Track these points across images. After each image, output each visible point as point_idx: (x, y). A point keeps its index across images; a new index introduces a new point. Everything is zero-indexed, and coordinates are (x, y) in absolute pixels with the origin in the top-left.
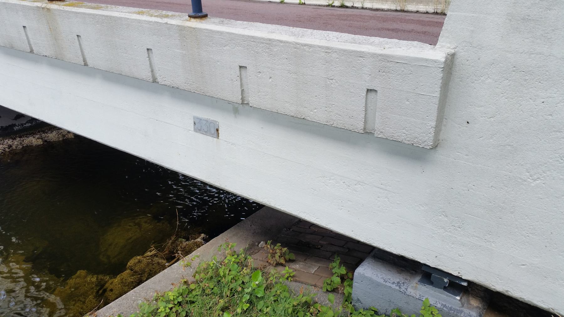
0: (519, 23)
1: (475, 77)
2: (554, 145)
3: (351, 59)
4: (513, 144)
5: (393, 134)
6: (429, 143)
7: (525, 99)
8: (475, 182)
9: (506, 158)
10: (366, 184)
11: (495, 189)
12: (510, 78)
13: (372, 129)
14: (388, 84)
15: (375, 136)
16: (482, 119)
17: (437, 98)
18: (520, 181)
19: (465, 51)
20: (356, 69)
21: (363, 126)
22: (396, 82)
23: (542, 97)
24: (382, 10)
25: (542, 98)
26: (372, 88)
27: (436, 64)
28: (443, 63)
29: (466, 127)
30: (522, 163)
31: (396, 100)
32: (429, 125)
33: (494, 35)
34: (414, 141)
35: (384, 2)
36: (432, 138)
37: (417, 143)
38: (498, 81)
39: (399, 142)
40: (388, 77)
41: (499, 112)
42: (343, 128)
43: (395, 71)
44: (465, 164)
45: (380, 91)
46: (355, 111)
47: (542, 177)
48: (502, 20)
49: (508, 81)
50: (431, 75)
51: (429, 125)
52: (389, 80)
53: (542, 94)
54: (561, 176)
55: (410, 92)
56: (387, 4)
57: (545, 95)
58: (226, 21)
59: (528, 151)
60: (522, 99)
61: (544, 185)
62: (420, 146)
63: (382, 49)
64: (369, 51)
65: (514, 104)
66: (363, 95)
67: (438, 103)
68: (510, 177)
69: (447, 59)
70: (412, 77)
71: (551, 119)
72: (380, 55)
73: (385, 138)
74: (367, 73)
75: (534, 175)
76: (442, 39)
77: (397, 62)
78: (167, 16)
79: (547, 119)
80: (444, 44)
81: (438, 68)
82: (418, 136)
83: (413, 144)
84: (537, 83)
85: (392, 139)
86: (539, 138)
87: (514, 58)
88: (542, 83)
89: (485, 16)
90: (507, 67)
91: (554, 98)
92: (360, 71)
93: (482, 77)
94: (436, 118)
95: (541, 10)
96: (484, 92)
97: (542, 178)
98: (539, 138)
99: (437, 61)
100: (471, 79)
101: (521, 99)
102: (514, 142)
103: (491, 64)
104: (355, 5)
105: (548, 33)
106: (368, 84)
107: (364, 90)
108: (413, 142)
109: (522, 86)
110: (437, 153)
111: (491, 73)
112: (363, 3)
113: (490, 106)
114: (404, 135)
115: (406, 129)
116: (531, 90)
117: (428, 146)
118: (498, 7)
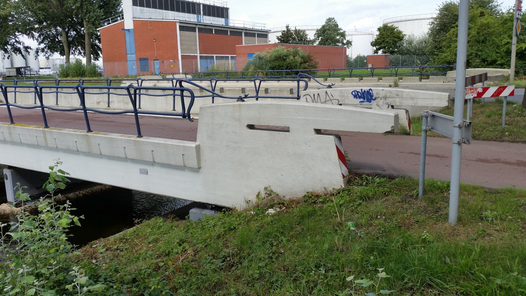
58: (148, 137)
78: (130, 137)
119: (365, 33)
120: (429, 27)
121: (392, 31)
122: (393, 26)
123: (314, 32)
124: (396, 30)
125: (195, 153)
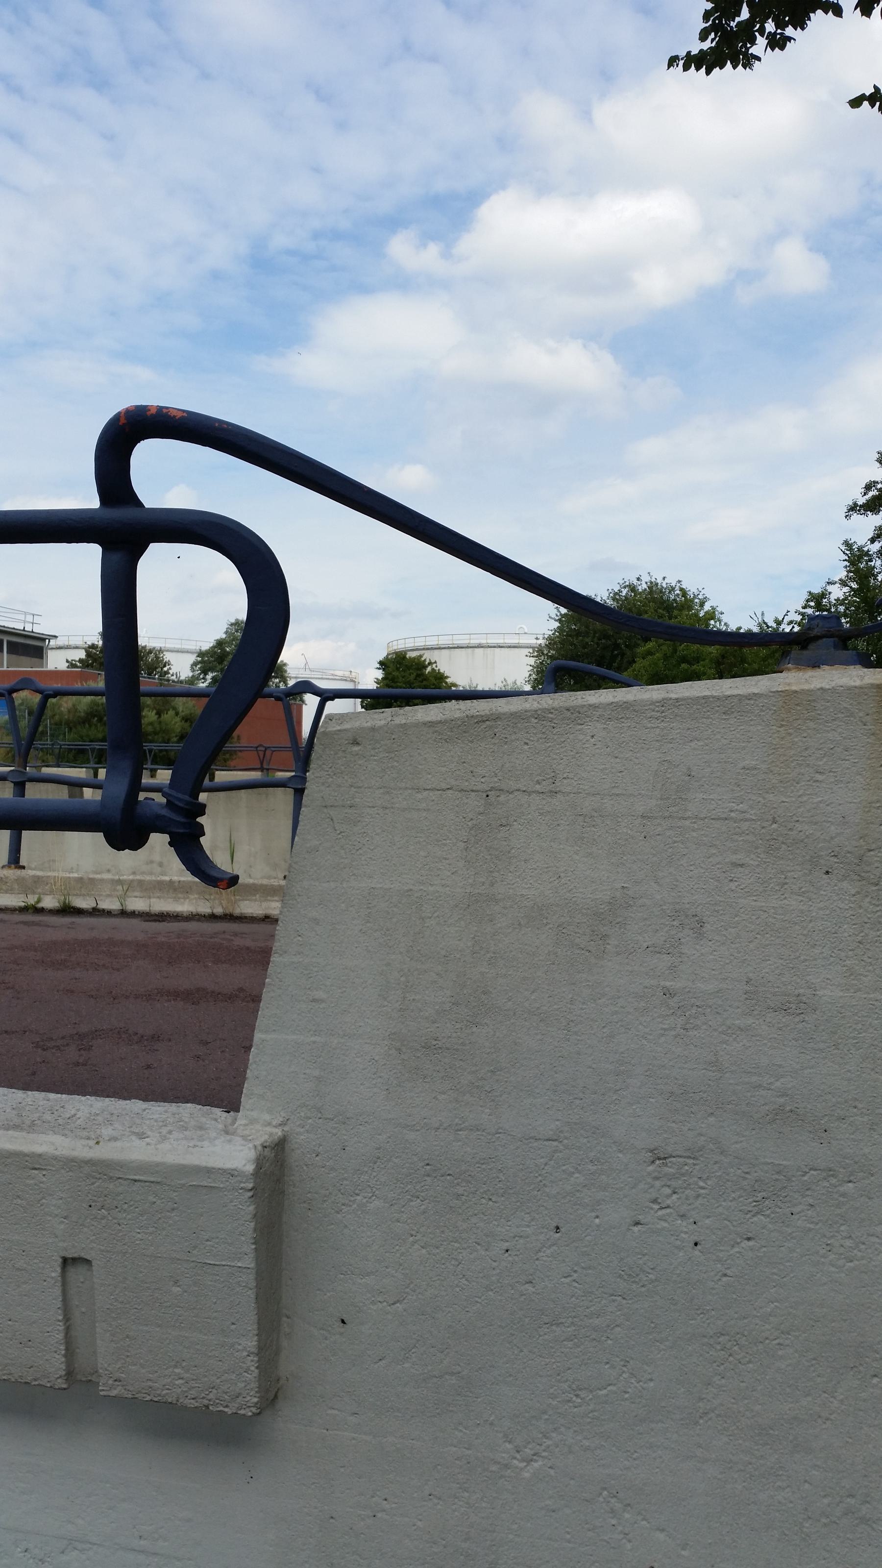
0: (418, 1057)
1: (341, 1196)
2: (553, 1360)
3: (9, 1176)
4: (459, 1369)
5: (150, 1383)
6: (249, 1398)
7: (465, 1246)
8: (388, 1488)
9: (451, 1409)
10: (95, 1544)
11: (441, 1503)
12: (422, 1194)
13: (92, 1371)
14: (117, 1241)
15: (102, 1393)
16: (375, 1307)
17: (249, 1271)
18: (494, 1468)
19: (307, 1131)
20: (24, 1203)
21: (63, 1367)
22: (139, 1233)
23: (501, 1238)
24: (176, 917)
25: (502, 1240)
26: (76, 1255)
27: (233, 1180)
28: (252, 1177)
29: (341, 1334)
30: (492, 1419)
31: (146, 1285)
32: (240, 1347)
33: (369, 1088)
34: (209, 1397)
35: (180, 895)
36: (254, 1385)
37: (217, 1401)
38: (396, 1204)
39: (171, 1403)
40: (116, 1221)
41: (412, 1286)
42: (5, 1377)
43: (132, 1203)
44: (354, 1441)
45: (99, 1262)
46: (34, 1323)
47: (544, 1451)
48: (382, 1051)
49: (419, 1201)
50: (224, 1209)
51: (240, 1347)
52: (120, 1228)
53: (499, 1229)
54: (584, 1441)
55: (179, 1259)
56: (187, 900)
57: (508, 1231)
59: (497, 1384)
60: (459, 1245)
61: (552, 1472)
62: (226, 1410)
63: (92, 1143)
64: (57, 1153)
65: (443, 1261)
66: (53, 1275)
67: (253, 1284)
68: (468, 1463)
69: (260, 1162)
70: (177, 1218)
71: (534, 1293)
72: (90, 1162)
73: (130, 1396)
74: (56, 1212)
75: (526, 1447)
76: (250, 1101)
77: (135, 1181)
79: (524, 1295)
80: (255, 1114)
81: (241, 1191)
82: (218, 1381)
83: (207, 1407)
84: (484, 1201)
85: (148, 1398)
86: (515, 1345)
87: (423, 1142)
88: (495, 1202)
89: (343, 1041)
90: (413, 1166)
91: (528, 1237)
92: (39, 1207)
93: (358, 1195)
94: (255, 1326)
95: (458, 1026)
96: (369, 1233)
97: (544, 1454)
98: (515, 1345)
99: (236, 1173)
100: (333, 1202)
101: (457, 1245)
102: (462, 1364)
103: (374, 1159)
104: (105, 905)
105: (483, 1079)
106: (65, 1244)
107: (56, 1261)
108: (207, 1402)
109: (454, 1212)
110: (279, 1419)
111: (378, 1183)
112: (122, 898)
113: (387, 1270)
114: (181, 1381)
115: (184, 1364)
116: (474, 1220)
117: (248, 1410)
118: (367, 1020)
119: (333, 675)
120: (532, 661)
121: (419, 672)
122: (423, 659)
123: (192, 658)
124: (429, 669)
125: (249, 1248)
